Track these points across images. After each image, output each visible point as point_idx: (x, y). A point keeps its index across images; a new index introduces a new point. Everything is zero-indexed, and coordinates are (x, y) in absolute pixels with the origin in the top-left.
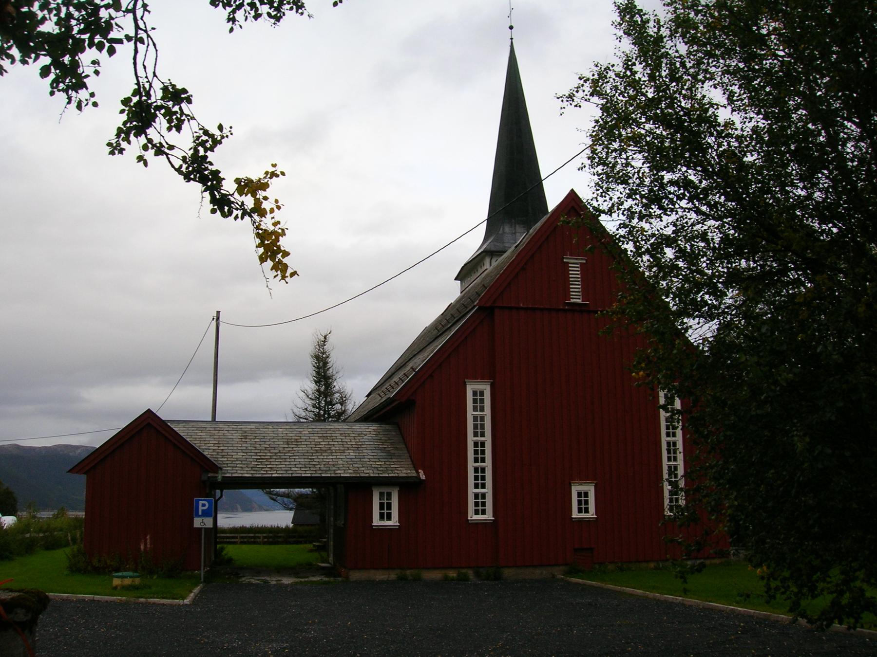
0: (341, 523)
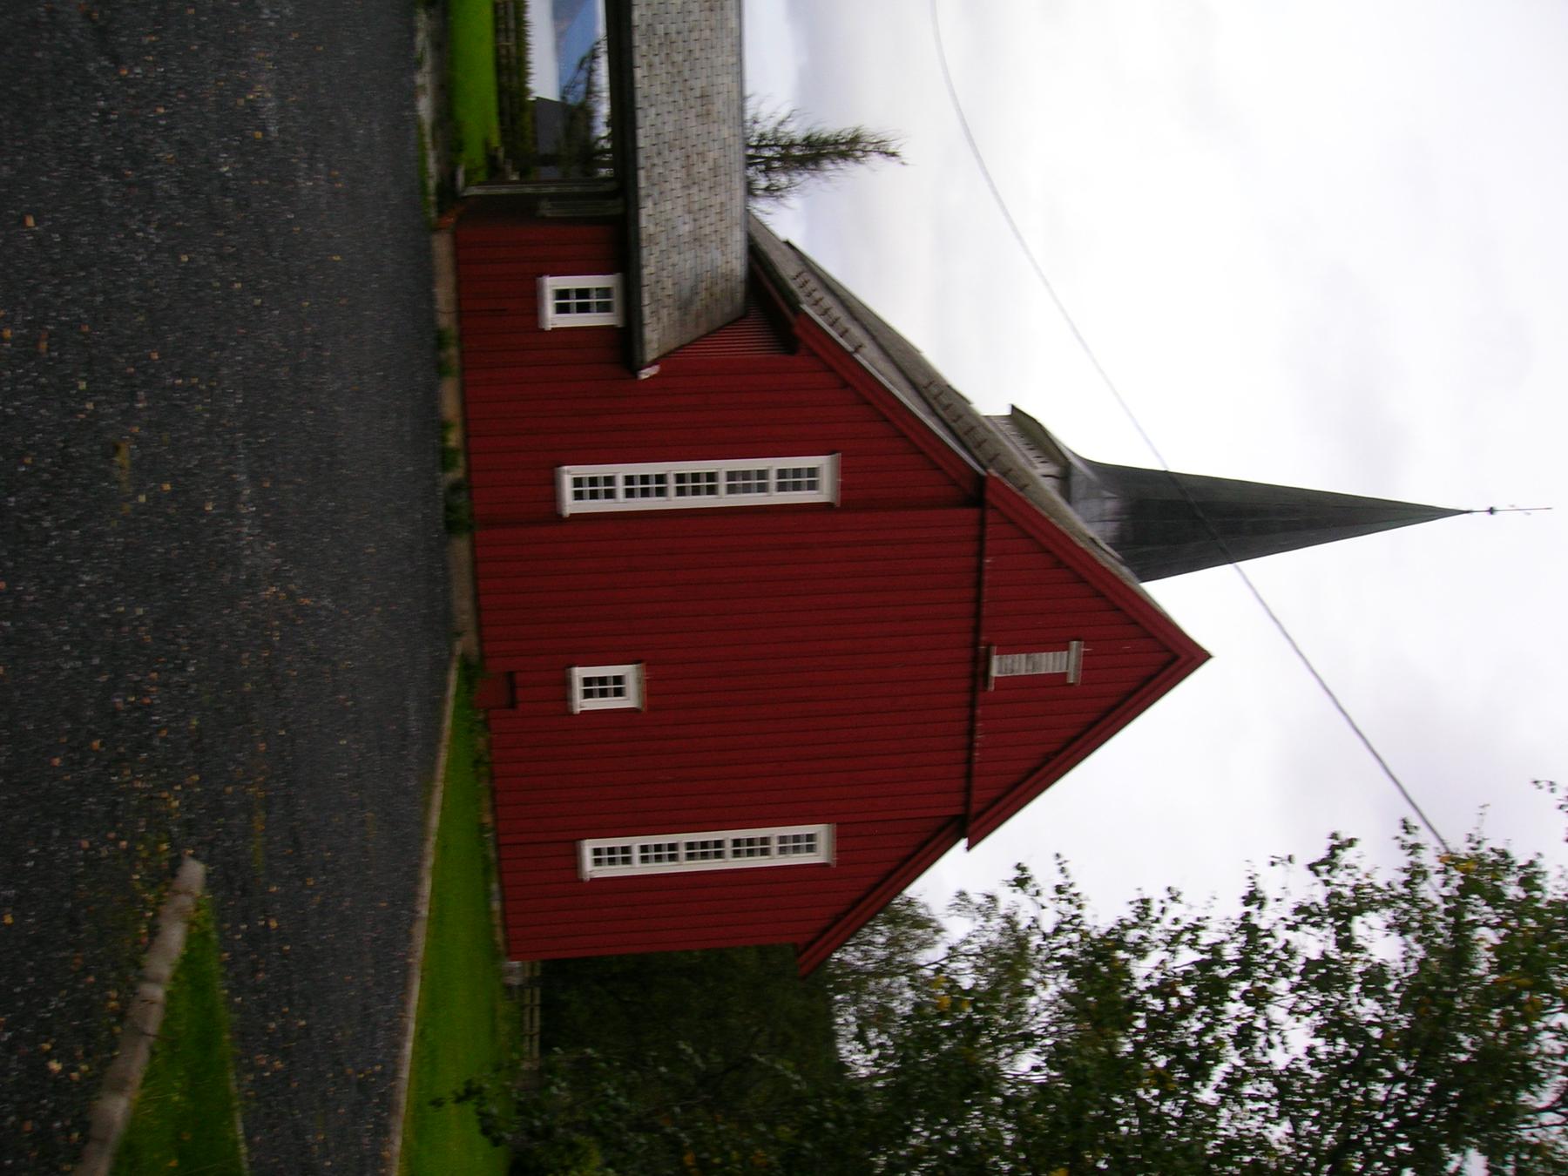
0: (546, 209)
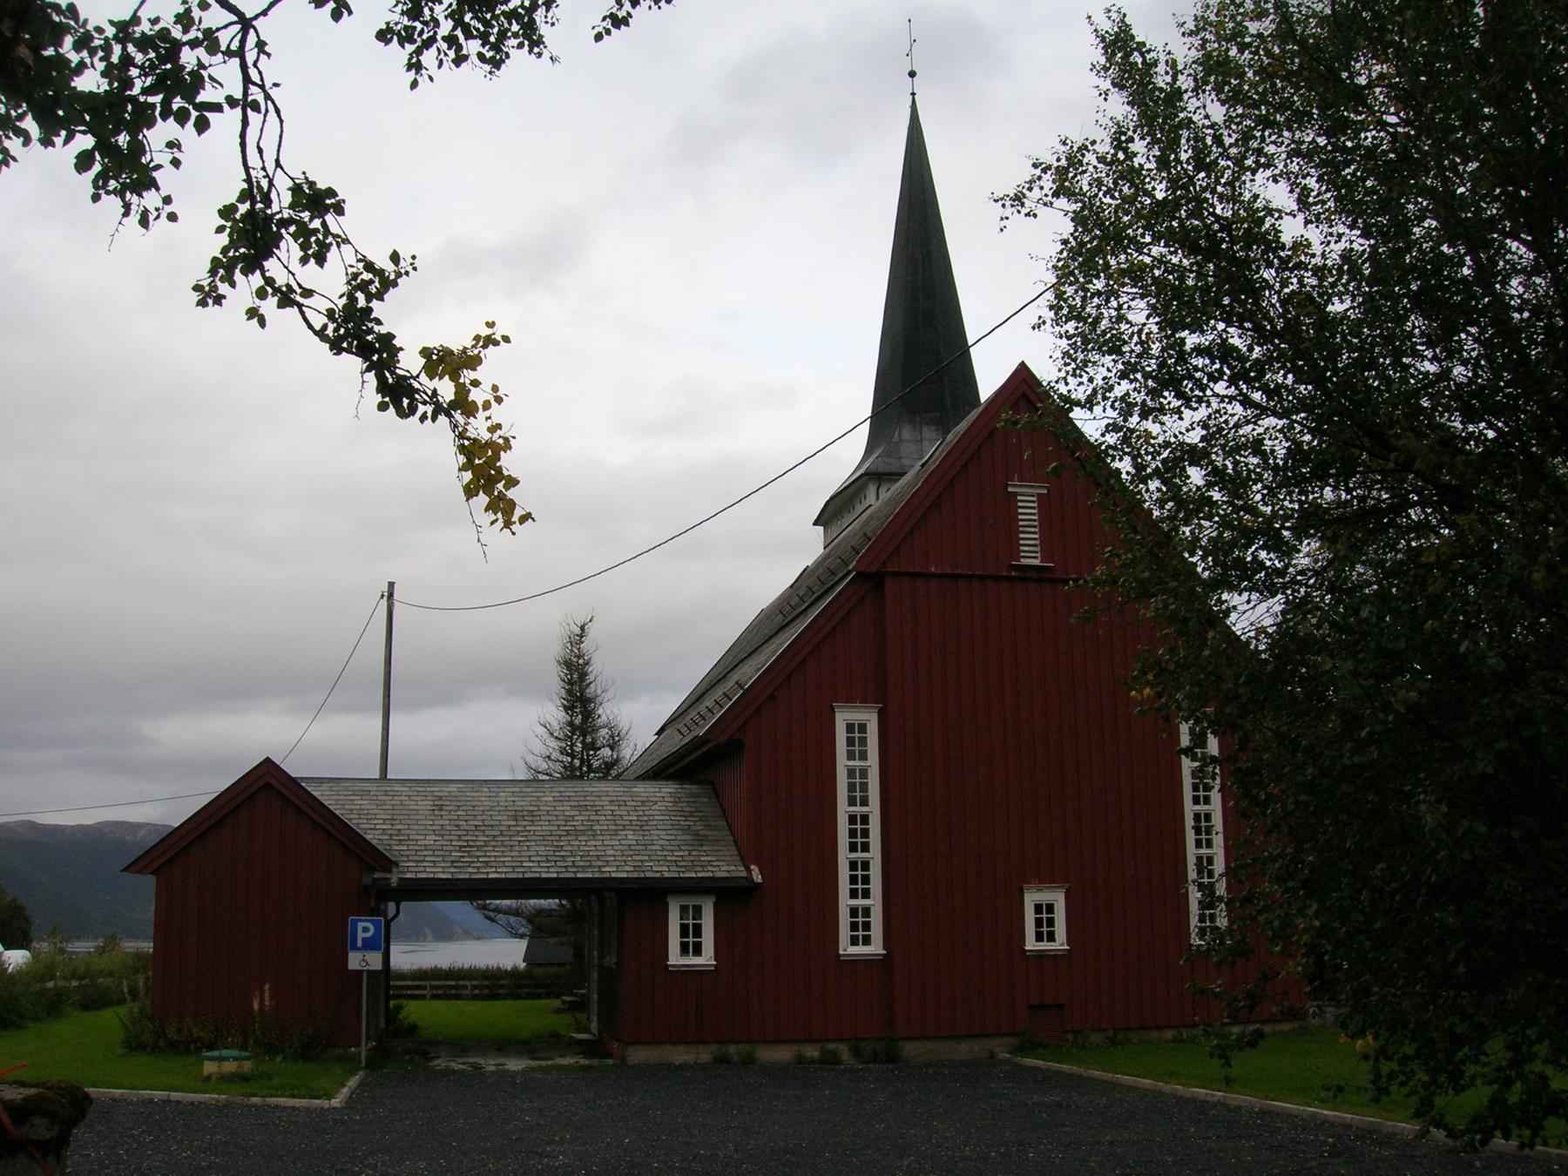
0: (611, 960)
